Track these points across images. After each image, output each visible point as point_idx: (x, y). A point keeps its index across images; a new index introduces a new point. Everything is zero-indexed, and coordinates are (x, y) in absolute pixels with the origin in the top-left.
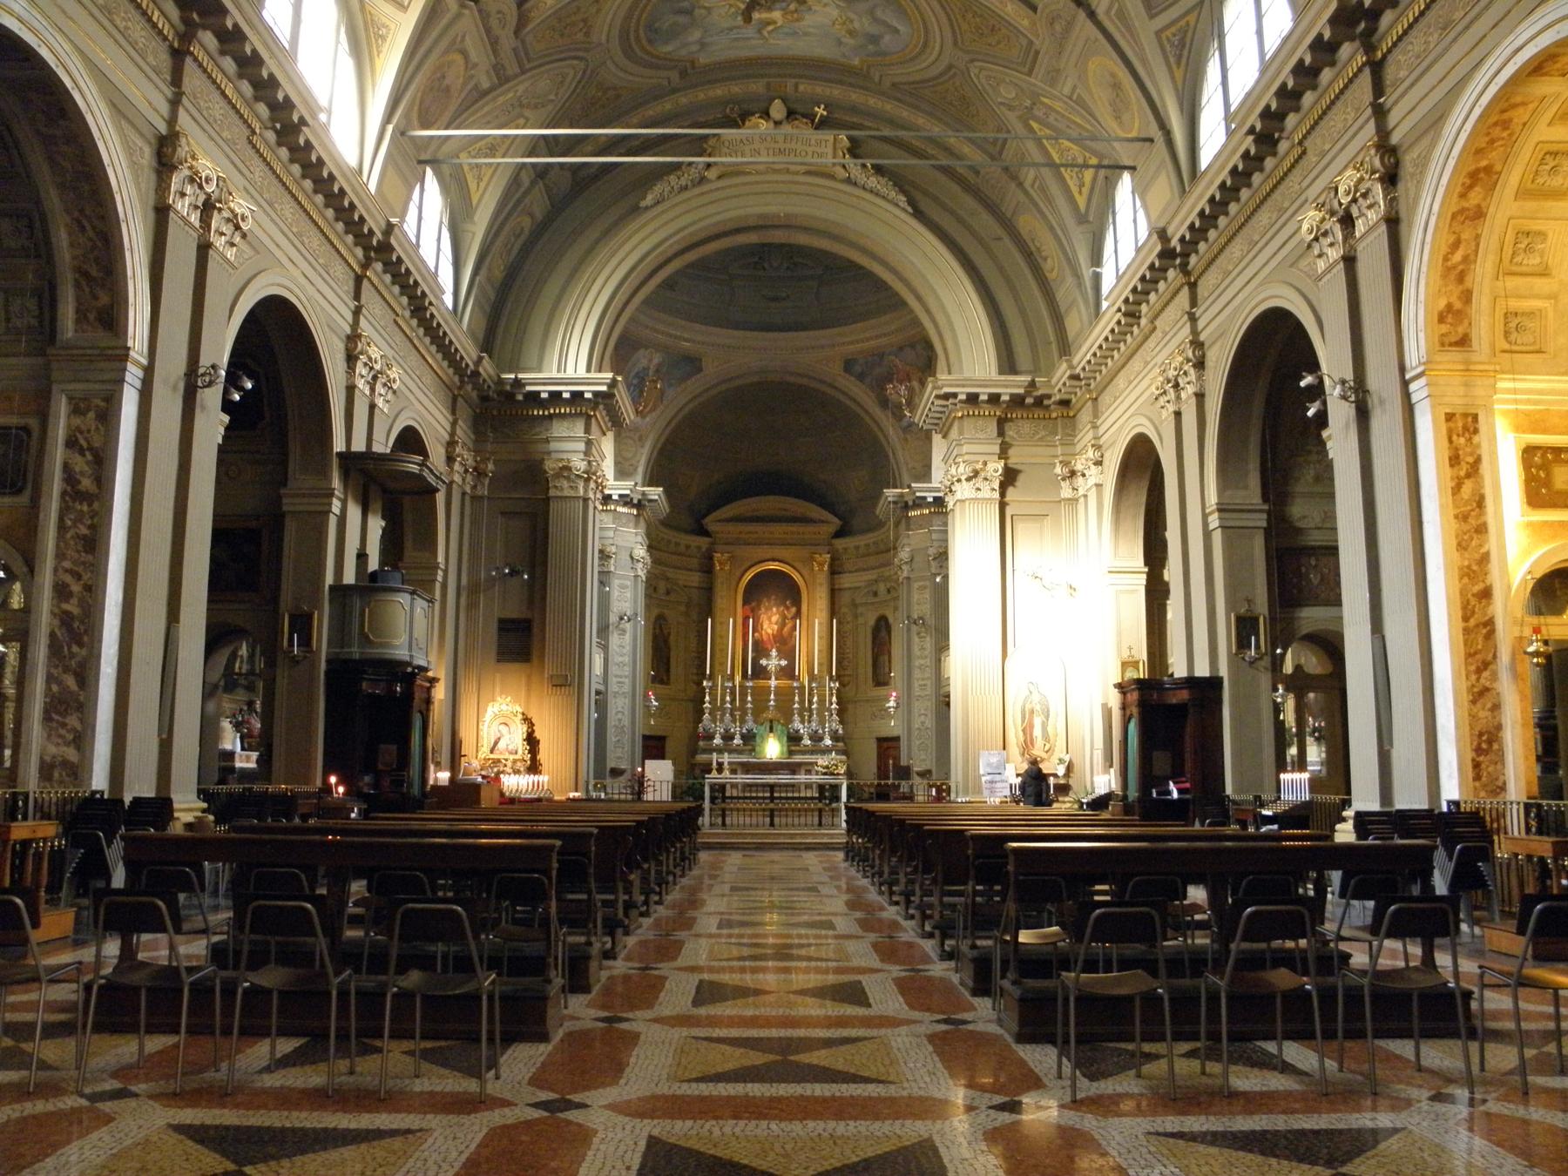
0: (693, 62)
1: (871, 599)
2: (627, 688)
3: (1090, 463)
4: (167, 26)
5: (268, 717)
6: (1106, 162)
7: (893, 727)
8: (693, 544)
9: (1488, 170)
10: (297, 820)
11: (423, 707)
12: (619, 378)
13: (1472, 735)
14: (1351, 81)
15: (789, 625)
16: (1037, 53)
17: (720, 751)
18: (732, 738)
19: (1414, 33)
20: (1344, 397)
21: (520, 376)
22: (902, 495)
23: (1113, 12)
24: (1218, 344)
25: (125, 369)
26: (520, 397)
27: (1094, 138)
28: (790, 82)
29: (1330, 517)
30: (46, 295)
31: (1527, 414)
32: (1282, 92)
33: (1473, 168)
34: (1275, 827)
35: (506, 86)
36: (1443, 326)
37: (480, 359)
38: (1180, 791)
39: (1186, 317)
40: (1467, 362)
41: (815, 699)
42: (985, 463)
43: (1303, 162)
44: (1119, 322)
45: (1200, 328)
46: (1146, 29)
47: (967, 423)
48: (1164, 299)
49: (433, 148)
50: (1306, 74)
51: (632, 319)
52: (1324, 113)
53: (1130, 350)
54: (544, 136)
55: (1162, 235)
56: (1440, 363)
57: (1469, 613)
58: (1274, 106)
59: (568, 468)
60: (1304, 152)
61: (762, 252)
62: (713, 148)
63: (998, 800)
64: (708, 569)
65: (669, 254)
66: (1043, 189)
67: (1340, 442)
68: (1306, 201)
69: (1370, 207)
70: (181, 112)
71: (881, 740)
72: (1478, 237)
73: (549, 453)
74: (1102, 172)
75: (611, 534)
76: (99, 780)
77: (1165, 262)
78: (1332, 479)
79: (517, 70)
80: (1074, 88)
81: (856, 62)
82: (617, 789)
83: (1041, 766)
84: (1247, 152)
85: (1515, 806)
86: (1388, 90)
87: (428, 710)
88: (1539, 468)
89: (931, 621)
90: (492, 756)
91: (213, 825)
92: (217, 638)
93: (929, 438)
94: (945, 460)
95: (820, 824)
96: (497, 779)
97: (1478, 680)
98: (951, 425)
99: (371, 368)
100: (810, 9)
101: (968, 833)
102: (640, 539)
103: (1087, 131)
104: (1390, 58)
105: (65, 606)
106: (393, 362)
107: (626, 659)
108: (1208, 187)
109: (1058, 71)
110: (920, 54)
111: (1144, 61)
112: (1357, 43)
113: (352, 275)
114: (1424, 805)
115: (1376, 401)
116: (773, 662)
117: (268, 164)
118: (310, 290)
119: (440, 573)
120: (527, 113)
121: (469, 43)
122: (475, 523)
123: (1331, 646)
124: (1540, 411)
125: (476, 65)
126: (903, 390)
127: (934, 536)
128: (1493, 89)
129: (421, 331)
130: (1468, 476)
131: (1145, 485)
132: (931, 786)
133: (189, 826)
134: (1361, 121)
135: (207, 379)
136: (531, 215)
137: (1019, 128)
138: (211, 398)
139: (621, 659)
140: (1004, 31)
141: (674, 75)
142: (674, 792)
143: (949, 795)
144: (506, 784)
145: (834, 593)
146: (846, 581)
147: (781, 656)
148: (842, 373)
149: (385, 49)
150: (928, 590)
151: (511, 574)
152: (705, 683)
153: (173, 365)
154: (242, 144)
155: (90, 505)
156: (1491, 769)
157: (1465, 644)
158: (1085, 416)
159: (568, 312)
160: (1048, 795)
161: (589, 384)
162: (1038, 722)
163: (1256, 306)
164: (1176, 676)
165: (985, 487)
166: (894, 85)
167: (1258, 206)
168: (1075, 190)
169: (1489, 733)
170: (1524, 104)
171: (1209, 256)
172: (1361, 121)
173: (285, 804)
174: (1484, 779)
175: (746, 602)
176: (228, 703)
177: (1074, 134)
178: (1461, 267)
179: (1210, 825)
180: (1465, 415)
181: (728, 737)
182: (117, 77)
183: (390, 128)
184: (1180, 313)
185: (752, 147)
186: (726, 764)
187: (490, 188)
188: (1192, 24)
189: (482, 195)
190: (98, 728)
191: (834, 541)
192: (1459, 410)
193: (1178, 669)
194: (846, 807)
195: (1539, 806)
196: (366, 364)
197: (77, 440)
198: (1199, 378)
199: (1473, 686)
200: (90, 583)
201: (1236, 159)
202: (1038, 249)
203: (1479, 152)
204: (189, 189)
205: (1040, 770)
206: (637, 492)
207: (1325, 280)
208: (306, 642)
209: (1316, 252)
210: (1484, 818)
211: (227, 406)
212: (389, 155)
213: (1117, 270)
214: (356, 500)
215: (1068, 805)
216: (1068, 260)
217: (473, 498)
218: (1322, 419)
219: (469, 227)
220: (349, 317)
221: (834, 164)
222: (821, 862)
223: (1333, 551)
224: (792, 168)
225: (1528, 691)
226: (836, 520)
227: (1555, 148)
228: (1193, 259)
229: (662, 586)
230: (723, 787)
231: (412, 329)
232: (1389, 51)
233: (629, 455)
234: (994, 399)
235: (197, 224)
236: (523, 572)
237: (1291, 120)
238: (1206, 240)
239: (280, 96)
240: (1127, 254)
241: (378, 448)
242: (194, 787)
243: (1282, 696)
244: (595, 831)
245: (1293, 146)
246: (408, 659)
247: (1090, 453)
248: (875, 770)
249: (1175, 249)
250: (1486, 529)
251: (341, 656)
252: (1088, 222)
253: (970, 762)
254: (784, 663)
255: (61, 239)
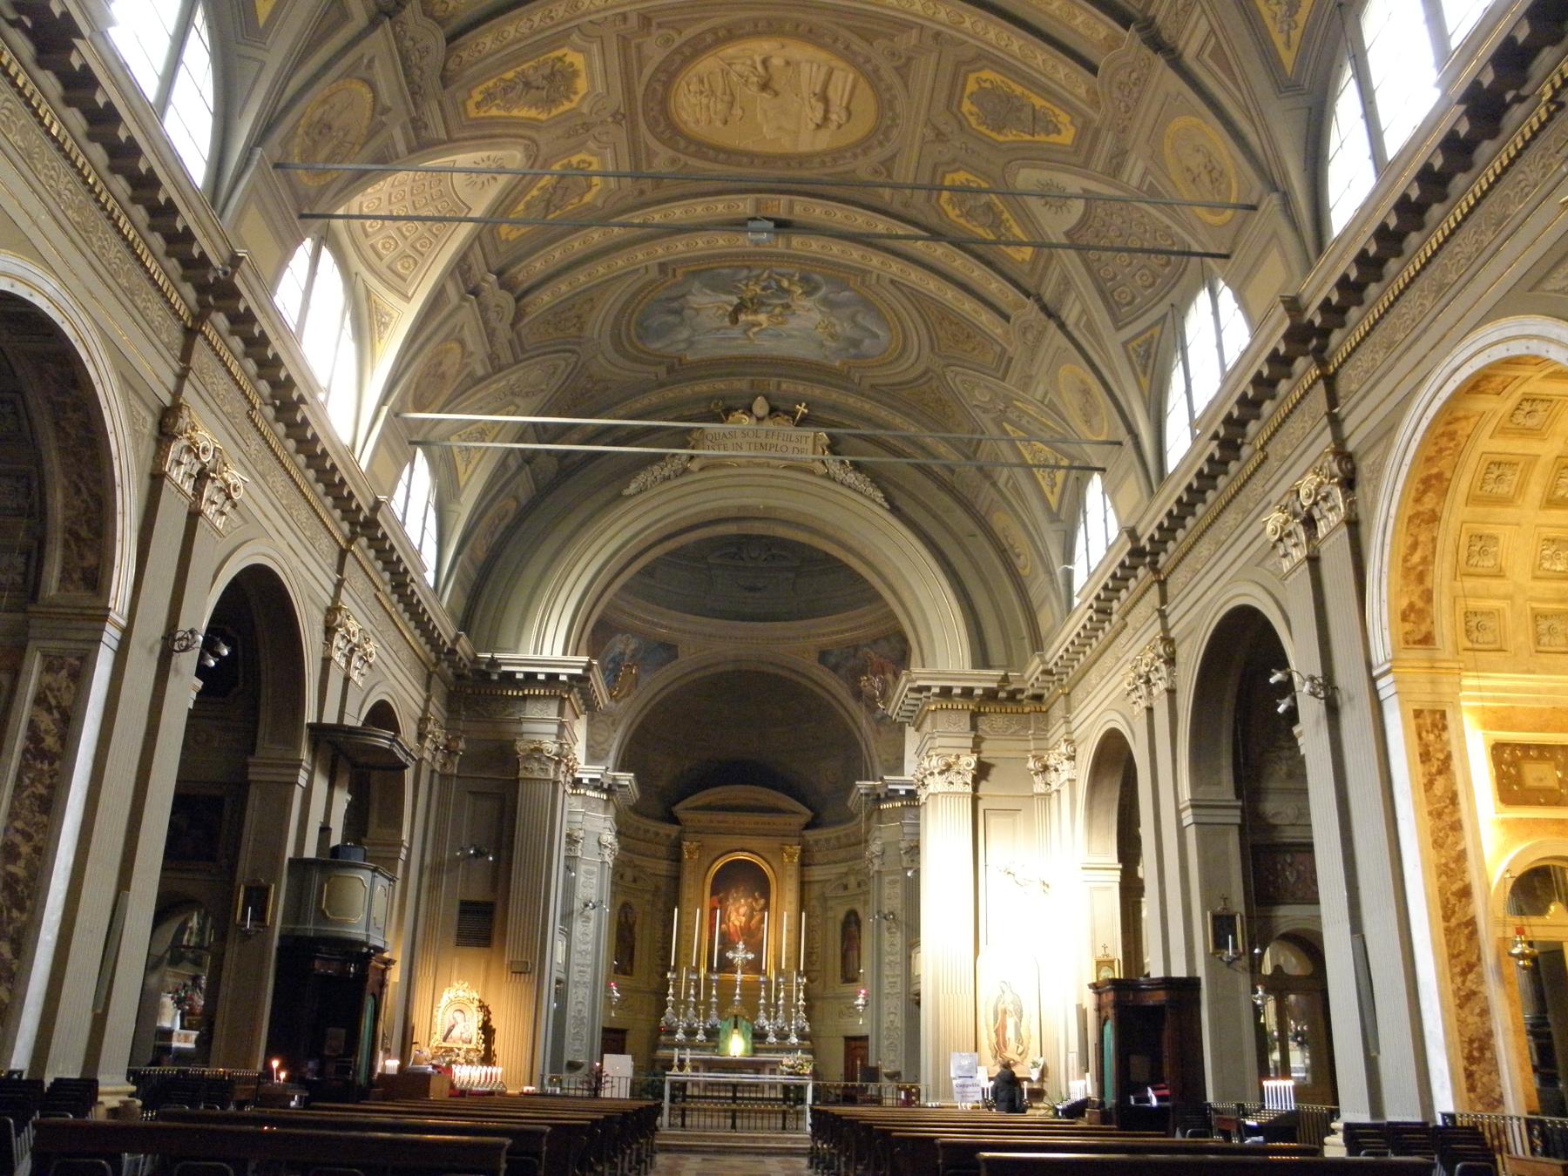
0: (680, 360)
1: (841, 893)
2: (588, 978)
3: (1063, 758)
4: (183, 307)
5: (212, 995)
6: (1076, 464)
7: (861, 1025)
8: (662, 832)
9: (1439, 476)
10: (232, 1108)
11: (377, 990)
12: (595, 662)
13: (1462, 1042)
14: (1306, 392)
15: (757, 918)
16: (1010, 360)
17: (682, 1046)
18: (695, 1033)
19: (1361, 350)
20: (1313, 694)
21: (497, 656)
22: (874, 787)
23: (1082, 324)
24: (1189, 640)
25: (103, 630)
26: (495, 677)
27: (1065, 441)
28: (774, 381)
29: (1304, 814)
30: (35, 554)
31: (1494, 711)
32: (1243, 401)
33: (1424, 474)
34: (1261, 1138)
35: (501, 374)
36: (1406, 624)
37: (458, 637)
38: (1159, 1098)
39: (1156, 614)
40: (1432, 660)
41: (782, 995)
42: (958, 757)
43: (1265, 467)
44: (1090, 619)
45: (1170, 625)
46: (1113, 341)
47: (940, 716)
48: (1134, 597)
49: (426, 429)
50: (1264, 385)
51: (610, 605)
52: (1284, 421)
53: (1101, 647)
54: (534, 424)
55: (1132, 534)
56: (1407, 660)
57: (1449, 912)
58: (1236, 414)
59: (539, 750)
60: (1266, 457)
61: (744, 541)
62: (697, 441)
63: (969, 1105)
64: (676, 857)
65: (651, 540)
66: (1017, 490)
67: (1311, 738)
68: (1269, 503)
69: (1331, 509)
70: (187, 387)
71: (848, 1039)
72: (1434, 540)
73: (522, 734)
74: (1074, 473)
75: (579, 818)
76: (20, 1059)
77: (1136, 561)
78: (1304, 776)
79: (511, 360)
80: (1046, 394)
81: (837, 364)
82: (573, 1084)
83: (1014, 1069)
84: (1212, 456)
85: (1515, 1121)
86: (1342, 402)
87: (381, 993)
88: (1510, 765)
89: (901, 916)
90: (444, 1044)
91: (139, 1110)
92: (166, 909)
93: (901, 729)
94: (918, 753)
95: (784, 1128)
96: (449, 1069)
97: (1464, 982)
98: (926, 716)
99: (349, 641)
100: (794, 313)
101: (938, 1141)
102: (608, 824)
103: (1059, 433)
104: (1342, 372)
105: (11, 868)
106: (371, 636)
107: (589, 947)
108: (1174, 490)
109: (1030, 377)
110: (897, 359)
111: (1113, 372)
112: (1310, 358)
113: (337, 548)
114: (1418, 1119)
115: (1345, 697)
116: (740, 955)
117: (264, 438)
118: (295, 561)
119: (404, 851)
120: (518, 400)
121: (467, 335)
122: (442, 803)
123: (1310, 946)
124: (1506, 708)
125: (472, 354)
126: (876, 682)
127: (906, 829)
128: (1437, 404)
129: (401, 607)
130: (1440, 772)
131: (1116, 794)
132: (900, 1089)
133: (113, 1112)
134: (1319, 427)
135: (184, 643)
136: (516, 499)
137: (993, 430)
138: (186, 663)
139: (583, 947)
140: (978, 338)
141: (662, 370)
142: (632, 1089)
143: (919, 1099)
144: (458, 1075)
145: (803, 885)
146: (816, 873)
147: (748, 949)
148: (817, 664)
149: (386, 335)
150: (898, 885)
151: (475, 855)
152: (669, 975)
153: (151, 628)
154: (241, 418)
155: (51, 764)
156: (1485, 1079)
157: (1448, 945)
158: (1057, 711)
159: (547, 594)
160: (1021, 1101)
161: (565, 667)
162: (1010, 1023)
163: (1221, 607)
164: (1152, 976)
165: (957, 780)
166: (873, 386)
167: (1224, 508)
168: (1047, 489)
169: (1480, 1040)
170: (1466, 418)
171: (1178, 555)
172: (1319, 427)
173: (220, 1089)
174: (1479, 1090)
175: (714, 892)
176: (172, 977)
177: (1046, 436)
178: (1420, 568)
179: (1192, 1135)
180: (1433, 712)
181: (691, 1032)
182: (131, 352)
183: (385, 409)
184: (1150, 611)
185: (735, 441)
186: (688, 1061)
187: (478, 471)
188: (1157, 335)
189: (469, 479)
190: (36, 962)
191: (805, 833)
192: (1427, 707)
193: (1155, 969)
194: (812, 1110)
195: (1542, 1123)
196: (343, 637)
197: (46, 696)
198: (1170, 674)
199: (1459, 989)
200: (40, 844)
201: (1201, 463)
202: (1012, 546)
203: (1429, 459)
204: (185, 459)
205: (1013, 1074)
206: (608, 776)
207: (1291, 578)
208: (260, 915)
209: (1281, 552)
210: (1483, 1134)
211: (202, 671)
212: (382, 435)
213: (1089, 568)
214: (323, 773)
215: (1043, 1112)
216: (1041, 557)
217: (443, 777)
218: (1292, 715)
219: (454, 507)
220: (331, 590)
221: (814, 460)
222: (784, 1168)
223: (1308, 848)
224: (773, 462)
225: (1517, 996)
226: (808, 812)
227: (1498, 458)
228: (1162, 558)
229: (629, 874)
230: (684, 1085)
231: (393, 605)
232: (1341, 366)
233: (600, 739)
234: (968, 693)
235: (190, 492)
236: (487, 855)
237: (1252, 427)
238: (1175, 539)
239: (282, 375)
240: (1098, 552)
241: (349, 721)
242: (125, 1068)
243: (1262, 998)
244: (548, 1129)
245: (1256, 450)
246: (364, 938)
247: (1063, 748)
248: (842, 1070)
249: (1144, 547)
250: (1461, 826)
251: (297, 933)
252: (1059, 520)
253: (941, 1065)
254: (750, 956)
255: (57, 500)
